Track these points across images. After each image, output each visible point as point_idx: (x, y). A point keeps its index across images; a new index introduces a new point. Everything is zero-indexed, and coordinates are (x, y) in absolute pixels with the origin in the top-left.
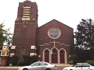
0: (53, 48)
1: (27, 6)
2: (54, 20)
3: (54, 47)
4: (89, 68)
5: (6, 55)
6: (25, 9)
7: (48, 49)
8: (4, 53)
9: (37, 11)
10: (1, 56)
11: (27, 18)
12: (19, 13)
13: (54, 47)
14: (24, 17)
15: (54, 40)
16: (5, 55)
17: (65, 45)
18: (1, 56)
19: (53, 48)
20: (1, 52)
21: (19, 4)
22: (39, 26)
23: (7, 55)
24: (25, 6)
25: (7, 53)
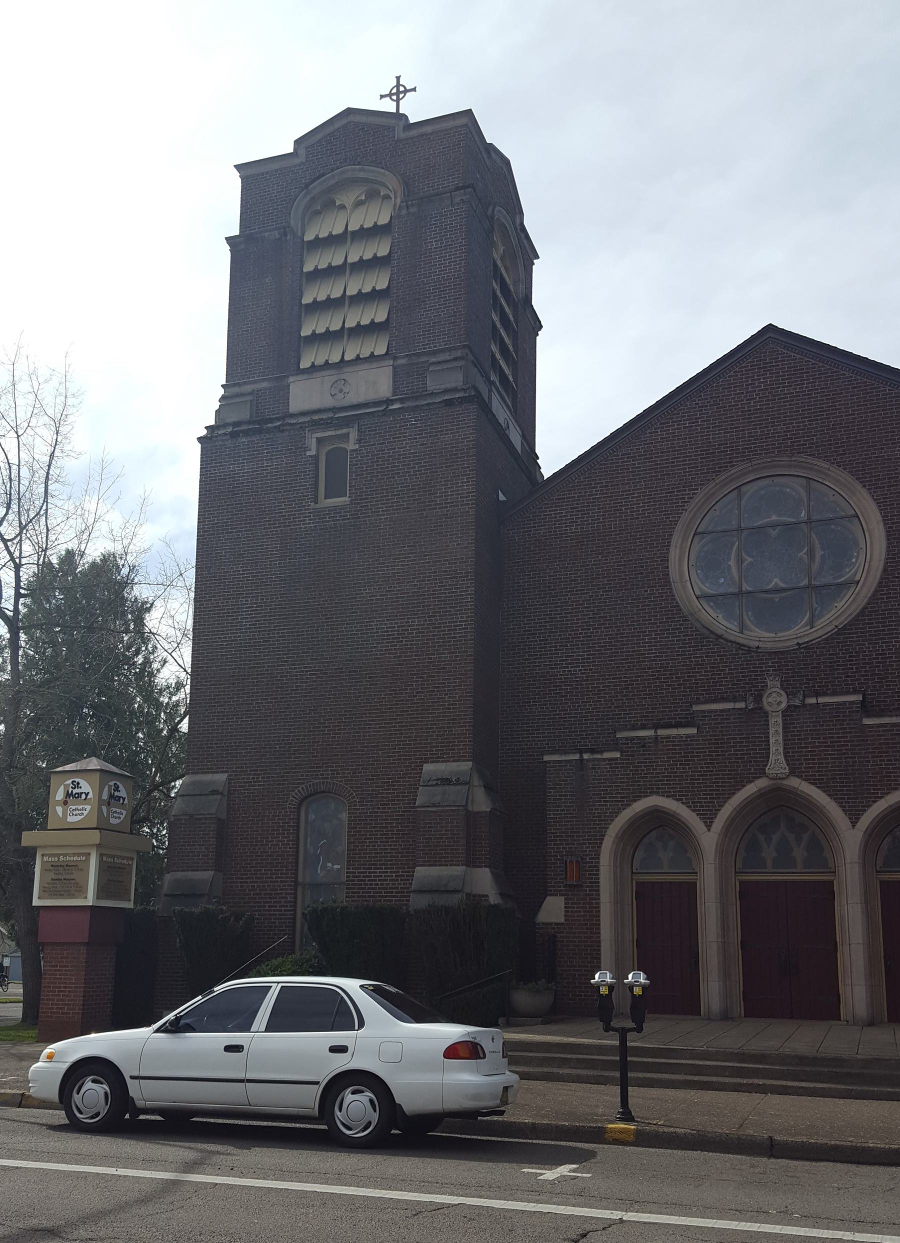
0: (751, 789)
1: (347, 198)
2: (770, 328)
3: (777, 763)
4: (335, 1049)
5: (90, 899)
6: (319, 244)
7: (625, 816)
8: (69, 866)
9: (521, 213)
10: (36, 902)
11: (348, 374)
12: (533, 362)
13: (777, 763)
14: (314, 368)
15: (778, 657)
16: (81, 890)
17: (866, 708)
18: (36, 902)
19: (751, 789)
20: (30, 853)
21: (234, 184)
22: (549, 465)
23: (103, 891)
24: (327, 205)
25: (105, 869)
